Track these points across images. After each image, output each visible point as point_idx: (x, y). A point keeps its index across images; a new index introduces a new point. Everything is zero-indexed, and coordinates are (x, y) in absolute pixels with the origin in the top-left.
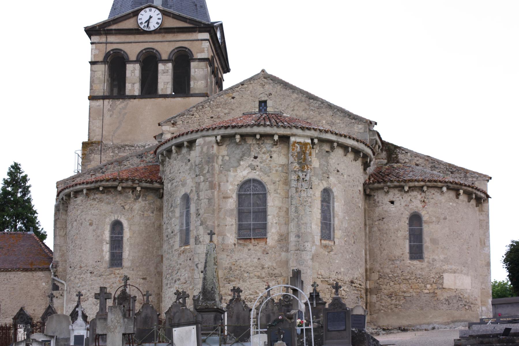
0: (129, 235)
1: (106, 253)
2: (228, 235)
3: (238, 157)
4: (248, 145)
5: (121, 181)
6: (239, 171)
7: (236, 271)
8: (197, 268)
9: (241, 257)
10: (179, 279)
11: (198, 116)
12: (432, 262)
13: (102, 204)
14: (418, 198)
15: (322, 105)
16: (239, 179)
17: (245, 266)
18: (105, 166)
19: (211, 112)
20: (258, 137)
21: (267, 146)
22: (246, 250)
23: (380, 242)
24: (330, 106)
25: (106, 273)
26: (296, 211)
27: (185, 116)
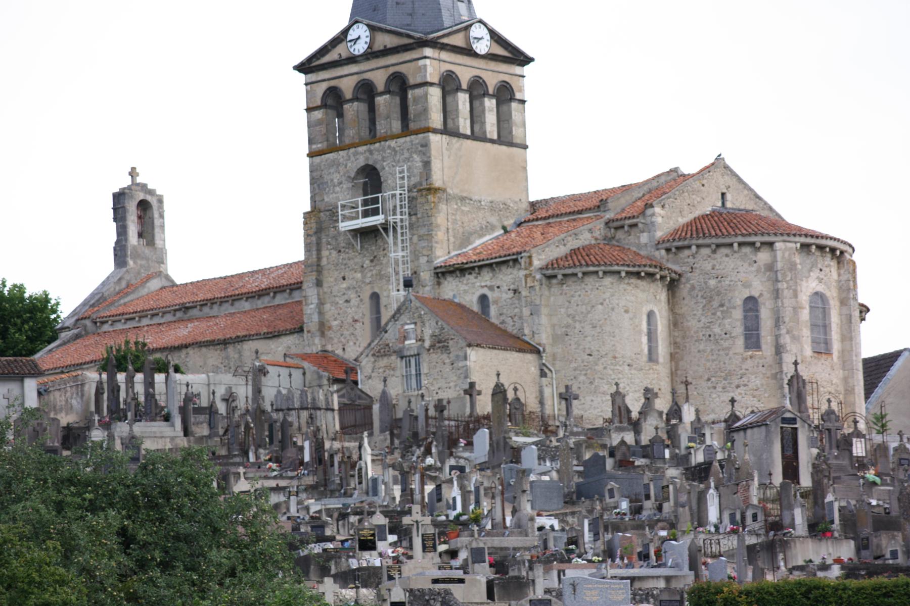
2: (806, 346)
10: (745, 385)
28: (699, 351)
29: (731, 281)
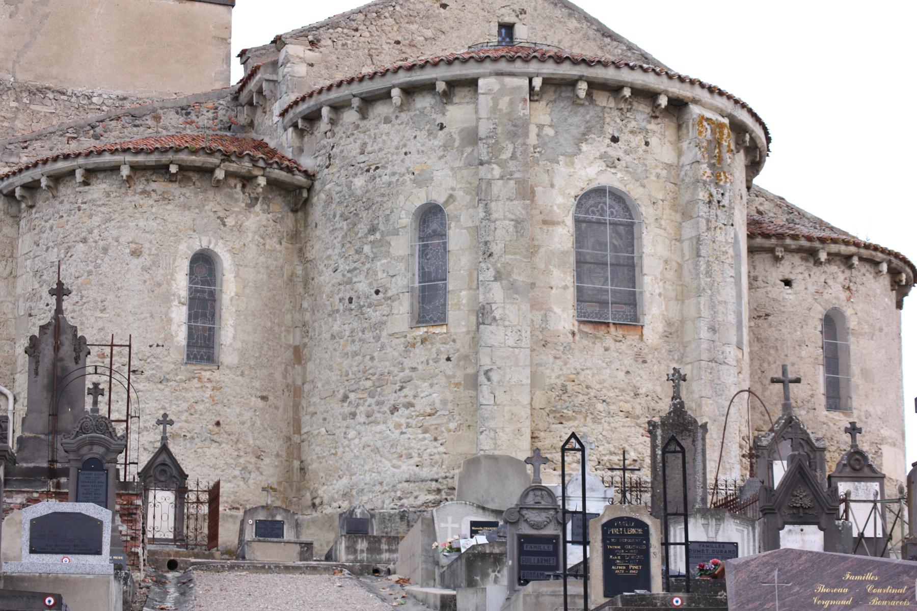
0: (235, 290)
1: (179, 326)
2: (557, 310)
3: (575, 132)
4: (598, 109)
5: (227, 157)
6: (578, 165)
7: (577, 396)
8: (489, 379)
9: (588, 364)
10: (410, 405)
11: (368, 34)
12: (864, 419)
13: (169, 207)
14: (838, 280)
15: (629, 54)
16: (577, 184)
17: (598, 387)
18: (102, 121)
19: (395, 28)
20: (627, 92)
21: (640, 117)
22: (599, 348)
23: (761, 365)
24: (646, 58)
25: (177, 375)
26: (707, 272)
27: (340, 30)
28: (333, 337)
29: (394, 174)
